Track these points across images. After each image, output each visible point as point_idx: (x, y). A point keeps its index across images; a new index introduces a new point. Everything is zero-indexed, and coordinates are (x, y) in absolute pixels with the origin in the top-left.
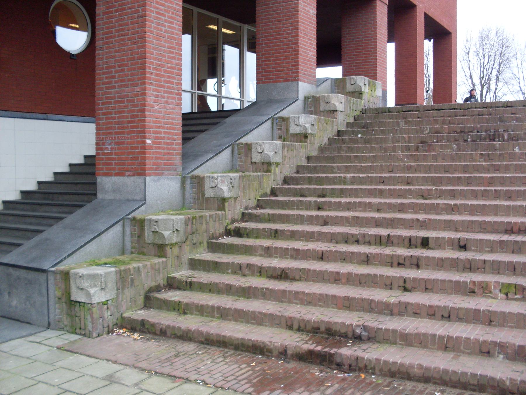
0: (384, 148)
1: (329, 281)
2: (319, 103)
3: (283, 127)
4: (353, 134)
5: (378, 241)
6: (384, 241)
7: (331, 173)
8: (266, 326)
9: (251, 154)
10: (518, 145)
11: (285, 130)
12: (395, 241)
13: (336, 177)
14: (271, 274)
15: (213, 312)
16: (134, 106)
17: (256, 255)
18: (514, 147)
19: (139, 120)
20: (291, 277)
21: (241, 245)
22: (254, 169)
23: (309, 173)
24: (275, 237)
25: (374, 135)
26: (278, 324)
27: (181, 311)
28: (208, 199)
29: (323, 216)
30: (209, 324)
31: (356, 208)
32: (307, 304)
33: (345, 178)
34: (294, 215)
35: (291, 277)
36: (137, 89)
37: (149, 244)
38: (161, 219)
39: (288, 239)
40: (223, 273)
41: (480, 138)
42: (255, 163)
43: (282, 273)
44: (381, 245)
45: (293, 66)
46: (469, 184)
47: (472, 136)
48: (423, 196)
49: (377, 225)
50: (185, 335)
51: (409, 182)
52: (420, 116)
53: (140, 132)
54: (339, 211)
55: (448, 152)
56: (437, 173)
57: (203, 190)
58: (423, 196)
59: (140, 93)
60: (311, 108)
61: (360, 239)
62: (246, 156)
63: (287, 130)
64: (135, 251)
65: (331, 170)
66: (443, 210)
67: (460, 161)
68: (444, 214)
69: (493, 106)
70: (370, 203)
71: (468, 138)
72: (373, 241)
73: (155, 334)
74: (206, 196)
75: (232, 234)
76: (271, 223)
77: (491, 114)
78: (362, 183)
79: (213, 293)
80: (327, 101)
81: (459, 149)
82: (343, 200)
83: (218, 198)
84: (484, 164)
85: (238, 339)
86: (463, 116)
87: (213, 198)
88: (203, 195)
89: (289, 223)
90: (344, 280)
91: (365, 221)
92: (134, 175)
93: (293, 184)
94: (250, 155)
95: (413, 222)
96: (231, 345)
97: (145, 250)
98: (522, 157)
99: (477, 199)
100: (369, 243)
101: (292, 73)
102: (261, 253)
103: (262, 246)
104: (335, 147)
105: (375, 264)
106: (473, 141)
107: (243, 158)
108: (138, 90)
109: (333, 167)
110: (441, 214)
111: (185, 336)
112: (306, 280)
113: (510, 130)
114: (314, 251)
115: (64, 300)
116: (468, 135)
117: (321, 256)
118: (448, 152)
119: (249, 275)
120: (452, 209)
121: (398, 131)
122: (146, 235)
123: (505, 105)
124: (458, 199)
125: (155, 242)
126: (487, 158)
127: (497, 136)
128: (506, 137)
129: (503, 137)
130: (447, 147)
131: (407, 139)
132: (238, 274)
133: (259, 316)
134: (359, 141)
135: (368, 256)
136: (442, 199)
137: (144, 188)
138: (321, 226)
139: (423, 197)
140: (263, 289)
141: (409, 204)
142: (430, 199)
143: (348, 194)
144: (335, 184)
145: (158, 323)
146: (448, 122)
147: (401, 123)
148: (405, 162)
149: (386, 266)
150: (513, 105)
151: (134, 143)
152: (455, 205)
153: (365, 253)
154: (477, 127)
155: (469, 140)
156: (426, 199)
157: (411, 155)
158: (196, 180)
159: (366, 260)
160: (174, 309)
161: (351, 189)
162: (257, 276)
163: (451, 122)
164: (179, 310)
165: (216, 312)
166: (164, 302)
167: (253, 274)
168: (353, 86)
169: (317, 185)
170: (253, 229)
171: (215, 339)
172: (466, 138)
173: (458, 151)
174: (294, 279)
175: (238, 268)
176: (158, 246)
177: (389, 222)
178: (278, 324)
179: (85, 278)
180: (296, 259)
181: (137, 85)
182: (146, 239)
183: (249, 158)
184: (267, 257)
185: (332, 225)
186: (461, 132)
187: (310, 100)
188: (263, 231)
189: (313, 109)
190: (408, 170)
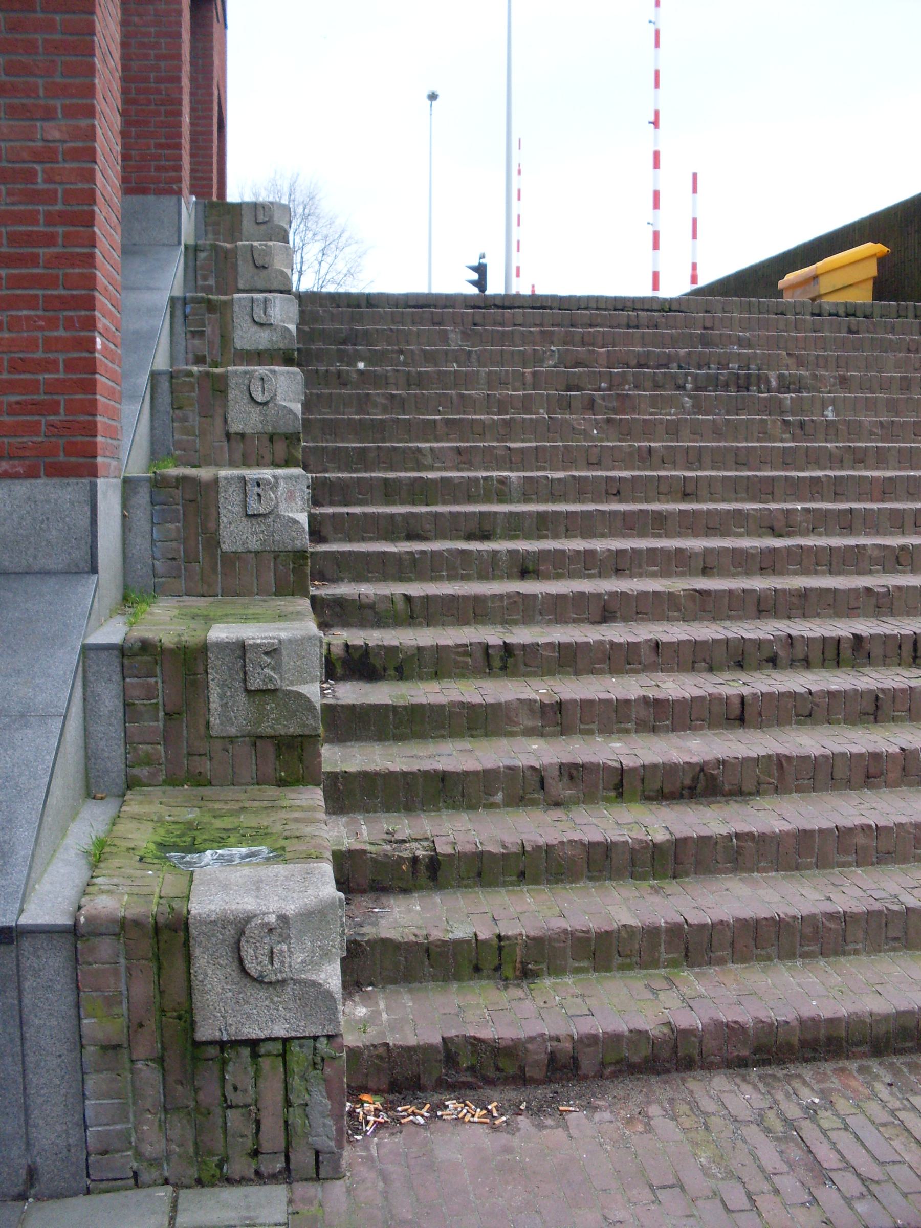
0: (499, 400)
1: (849, 784)
2: (235, 267)
3: (208, 330)
4: (341, 361)
5: (831, 653)
6: (846, 652)
7: (413, 470)
8: (856, 952)
9: (225, 406)
10: (833, 402)
11: (217, 340)
12: (877, 651)
13: (477, 479)
14: (657, 786)
15: (654, 946)
16: (34, 196)
17: (512, 734)
18: (824, 407)
19: (58, 256)
20: (727, 787)
21: (452, 704)
22: (238, 456)
23: (340, 470)
24: (504, 668)
25: (405, 364)
26: (896, 939)
27: (508, 971)
28: (232, 560)
29: (599, 595)
30: (705, 994)
31: (640, 566)
32: (879, 862)
33: (503, 481)
34: (501, 597)
35: (727, 787)
36: (54, 131)
37: (231, 739)
38: (290, 641)
39: (551, 673)
40: (472, 807)
41: (715, 382)
42: (242, 436)
43: (695, 779)
44: (838, 665)
45: (160, 146)
46: (837, 496)
47: (696, 377)
48: (772, 528)
49: (760, 612)
50: (665, 1054)
51: (688, 491)
52: (478, 319)
53: (65, 303)
54: (590, 576)
55: (670, 415)
56: (719, 469)
57: (211, 525)
58: (772, 528)
59: (61, 147)
60: (205, 278)
61: (781, 653)
62: (206, 413)
63: (225, 338)
64: (153, 775)
65: (416, 460)
66: (874, 561)
67: (736, 440)
68: (877, 571)
69: (637, 306)
70: (679, 551)
71: (686, 381)
72: (815, 655)
73: (521, 1079)
74: (225, 547)
75: (339, 671)
76: (420, 625)
77: (656, 327)
78: (553, 497)
79: (536, 881)
80: (259, 262)
81: (698, 407)
82: (599, 545)
83: (276, 555)
84: (829, 445)
85: (886, 1017)
86: (591, 326)
87: (257, 553)
88: (213, 542)
89: (483, 623)
90: (893, 775)
91: (726, 600)
92: (31, 474)
93: (332, 504)
94: (220, 411)
95: (857, 598)
96: (858, 1044)
97: (205, 766)
98: (875, 430)
99: (903, 533)
100: (807, 663)
101: (158, 169)
102: (530, 724)
103: (530, 702)
104: (350, 395)
105: (894, 719)
106: (698, 389)
107: (194, 419)
108: (57, 135)
109: (419, 450)
110: (870, 572)
111: (669, 1058)
112: (776, 790)
113: (752, 367)
114: (714, 699)
115: (146, 1045)
116: (686, 375)
117: (737, 711)
118: (671, 414)
119: (577, 802)
120: (897, 558)
121: (474, 356)
122: (215, 704)
123: (667, 307)
124: (859, 534)
125: (265, 729)
126: (798, 431)
127: (753, 380)
128: (774, 383)
129: (768, 382)
130: (671, 402)
131: (529, 379)
132: (534, 803)
133: (832, 925)
134: (392, 380)
135: (877, 697)
136: (820, 535)
137: (86, 522)
138: (593, 623)
139: (775, 532)
140: (729, 837)
141: (788, 549)
142: (789, 535)
143: (562, 529)
144: (470, 499)
145: (532, 1039)
146: (578, 338)
147: (452, 336)
148: (593, 439)
149: (862, 722)
150: (682, 308)
151: (32, 344)
152: (903, 548)
153: (871, 691)
154: (677, 354)
155: (689, 386)
156: (780, 536)
157: (609, 421)
158: (178, 493)
159: (871, 709)
160: (477, 969)
161: (569, 514)
162: (607, 800)
163: (586, 339)
164: (498, 968)
165: (662, 949)
166: (427, 950)
167: (589, 798)
168: (263, 227)
169: (414, 503)
170: (419, 649)
171: (795, 1040)
172: (681, 382)
173: (695, 414)
174: (739, 793)
175: (534, 780)
176: (278, 747)
177: (795, 600)
178: (896, 939)
179: (293, 932)
180: (654, 730)
181: (49, 115)
182: (214, 721)
183: (219, 421)
184: (553, 735)
185: (626, 619)
186: (640, 366)
187: (202, 255)
188: (458, 654)
189: (211, 282)
190: (642, 459)
